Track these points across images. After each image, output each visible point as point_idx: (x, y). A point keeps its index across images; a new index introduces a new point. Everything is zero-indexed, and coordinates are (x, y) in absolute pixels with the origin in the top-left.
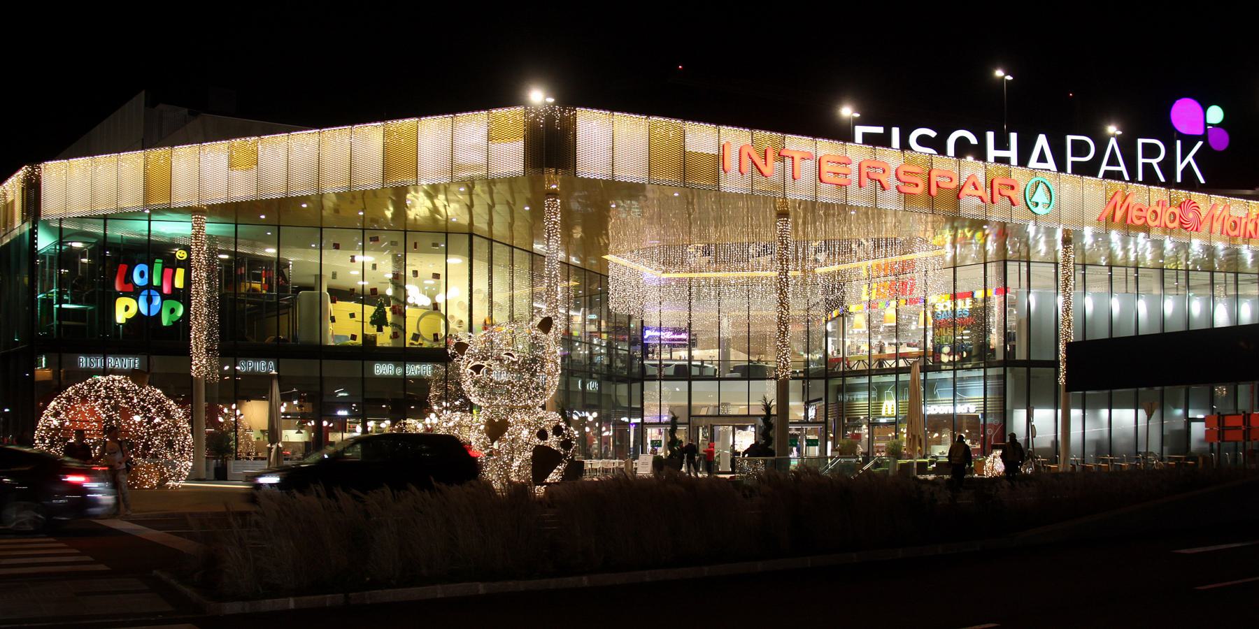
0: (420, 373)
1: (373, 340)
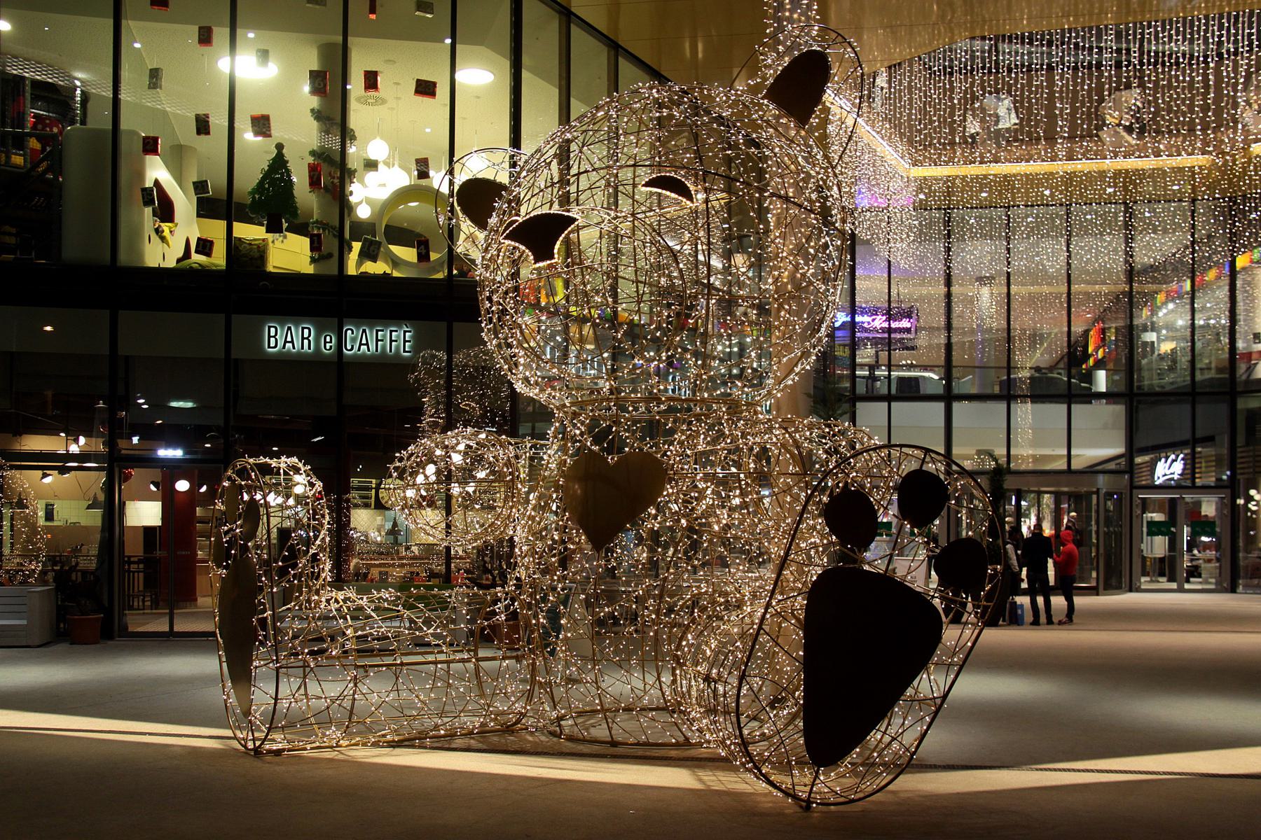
0: (384, 347)
1: (257, 255)
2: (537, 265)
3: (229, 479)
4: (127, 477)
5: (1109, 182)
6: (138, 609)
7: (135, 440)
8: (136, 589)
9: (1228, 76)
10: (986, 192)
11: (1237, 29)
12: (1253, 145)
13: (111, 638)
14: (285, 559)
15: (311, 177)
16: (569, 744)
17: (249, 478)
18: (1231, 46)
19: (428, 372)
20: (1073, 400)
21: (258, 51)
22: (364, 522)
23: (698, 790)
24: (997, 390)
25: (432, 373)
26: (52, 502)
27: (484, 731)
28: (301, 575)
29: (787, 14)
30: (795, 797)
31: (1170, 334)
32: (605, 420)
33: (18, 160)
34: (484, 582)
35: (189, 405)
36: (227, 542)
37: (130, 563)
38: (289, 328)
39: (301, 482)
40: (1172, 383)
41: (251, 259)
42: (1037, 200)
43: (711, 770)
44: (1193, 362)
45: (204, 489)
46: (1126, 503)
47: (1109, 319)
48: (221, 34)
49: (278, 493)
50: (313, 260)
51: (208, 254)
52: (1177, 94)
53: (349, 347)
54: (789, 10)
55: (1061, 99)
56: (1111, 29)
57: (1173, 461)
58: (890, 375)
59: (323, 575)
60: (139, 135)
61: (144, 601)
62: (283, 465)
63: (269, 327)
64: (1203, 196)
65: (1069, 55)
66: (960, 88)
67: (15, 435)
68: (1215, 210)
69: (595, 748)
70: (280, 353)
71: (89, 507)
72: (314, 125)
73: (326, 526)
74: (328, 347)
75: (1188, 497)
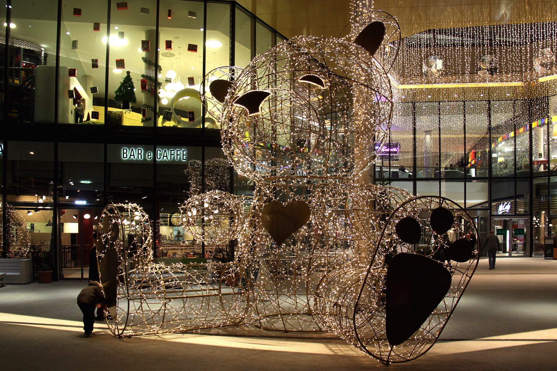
0: (174, 157)
1: (118, 118)
2: (251, 115)
3: (105, 213)
4: (63, 213)
5: (482, 92)
6: (69, 268)
7: (67, 197)
8: (68, 260)
9: (535, 48)
10: (431, 95)
11: (537, 29)
12: (540, 78)
13: (56, 280)
14: (131, 249)
15: (142, 85)
16: (265, 331)
17: (114, 213)
18: (536, 36)
19: (193, 169)
20: (467, 180)
21: (120, 32)
22: (164, 230)
23: (332, 355)
24: (433, 176)
25: (194, 170)
26: (33, 223)
27: (225, 326)
28: (139, 256)
29: (361, 9)
30: (381, 359)
31: (502, 154)
32: (278, 187)
33: (17, 82)
34: (219, 257)
35: (89, 182)
36: (104, 242)
37: (65, 248)
38: (132, 150)
39: (138, 215)
40: (506, 173)
41: (116, 120)
42: (453, 99)
43: (335, 344)
44: (515, 164)
45: (96, 218)
46: (489, 221)
47: (478, 148)
48: (103, 26)
49: (128, 220)
50: (143, 121)
51: (97, 118)
52: (515, 54)
53: (159, 158)
54: (361, 8)
55: (467, 55)
56: (487, 28)
57: (506, 205)
58: (390, 170)
59: (149, 257)
60: (67, 68)
61: (71, 264)
62: (130, 207)
63: (124, 149)
64: (520, 98)
65: (470, 38)
66: (424, 50)
67: (17, 195)
68: (525, 104)
69: (278, 334)
70: (128, 160)
71: (47, 225)
72: (143, 64)
73: (150, 235)
74: (149, 157)
75: (514, 219)
